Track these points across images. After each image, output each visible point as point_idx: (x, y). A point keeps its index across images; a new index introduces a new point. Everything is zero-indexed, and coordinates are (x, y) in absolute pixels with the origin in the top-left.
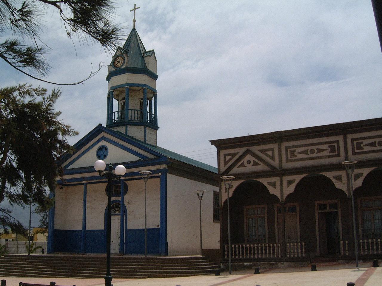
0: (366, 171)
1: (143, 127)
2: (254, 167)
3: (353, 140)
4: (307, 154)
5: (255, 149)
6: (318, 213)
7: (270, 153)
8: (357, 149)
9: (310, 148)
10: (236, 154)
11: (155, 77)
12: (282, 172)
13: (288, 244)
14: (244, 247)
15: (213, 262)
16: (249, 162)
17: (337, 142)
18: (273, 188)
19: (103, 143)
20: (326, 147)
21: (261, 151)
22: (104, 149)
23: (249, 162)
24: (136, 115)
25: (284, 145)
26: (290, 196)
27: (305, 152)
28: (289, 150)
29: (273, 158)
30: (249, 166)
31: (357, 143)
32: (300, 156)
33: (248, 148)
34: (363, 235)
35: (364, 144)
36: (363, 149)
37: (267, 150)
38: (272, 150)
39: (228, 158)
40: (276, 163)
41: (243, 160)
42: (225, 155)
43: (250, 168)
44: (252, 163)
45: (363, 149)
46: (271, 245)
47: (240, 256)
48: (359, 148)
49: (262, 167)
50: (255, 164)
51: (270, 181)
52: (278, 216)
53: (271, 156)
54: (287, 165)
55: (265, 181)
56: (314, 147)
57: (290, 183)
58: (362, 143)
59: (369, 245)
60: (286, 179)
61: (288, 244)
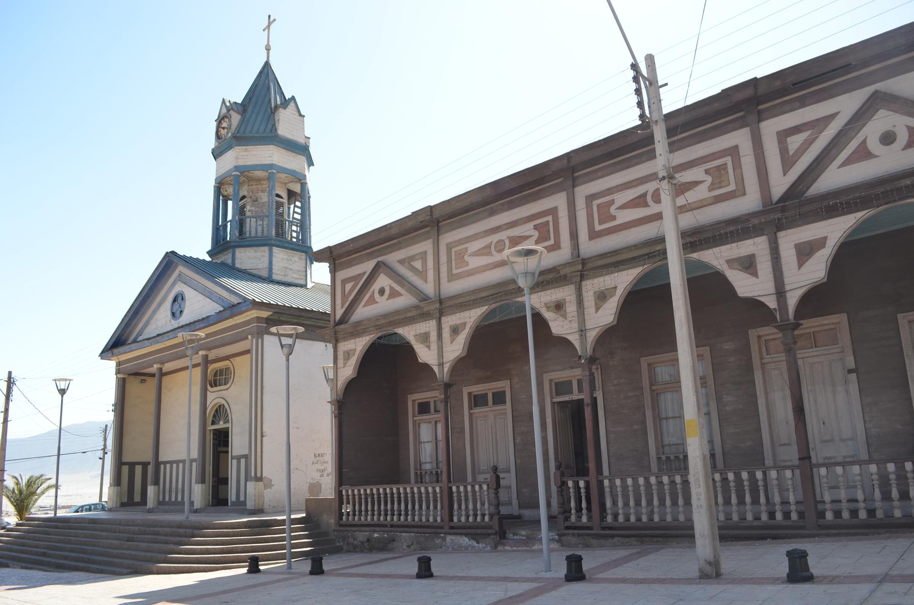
0: (835, 230)
1: (266, 249)
2: (391, 301)
3: (590, 198)
4: (489, 254)
5: (393, 258)
6: (553, 404)
7: (418, 264)
8: (600, 223)
9: (494, 238)
10: (827, 120)
11: (302, 149)
12: (443, 306)
13: (823, 471)
14: (742, 481)
15: (327, 539)
16: (888, 138)
17: (734, 151)
18: (426, 349)
19: (180, 287)
20: (527, 229)
21: (401, 262)
22: (180, 298)
23: (888, 138)
24: (260, 228)
25: (771, 127)
26: (607, 334)
27: (485, 251)
28: (453, 250)
29: (422, 274)
30: (379, 304)
31: (598, 206)
32: (475, 262)
33: (379, 259)
34: (659, 459)
35: (618, 203)
36: (614, 218)
37: (412, 258)
38: (423, 256)
39: (349, 286)
40: (429, 288)
41: (371, 290)
42: (344, 282)
43: (384, 305)
44: (387, 292)
45: (614, 218)
46: (641, 481)
47: (581, 517)
48: (607, 216)
49: (405, 300)
50: (394, 294)
51: (418, 332)
52: (471, 415)
53: (791, 153)
54: (450, 288)
55: (409, 333)
56: (503, 235)
57: (602, 297)
58: (612, 202)
59: (891, 485)
60: (591, 287)
61: (858, 467)
